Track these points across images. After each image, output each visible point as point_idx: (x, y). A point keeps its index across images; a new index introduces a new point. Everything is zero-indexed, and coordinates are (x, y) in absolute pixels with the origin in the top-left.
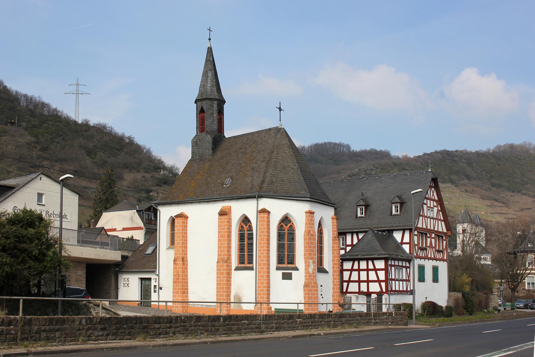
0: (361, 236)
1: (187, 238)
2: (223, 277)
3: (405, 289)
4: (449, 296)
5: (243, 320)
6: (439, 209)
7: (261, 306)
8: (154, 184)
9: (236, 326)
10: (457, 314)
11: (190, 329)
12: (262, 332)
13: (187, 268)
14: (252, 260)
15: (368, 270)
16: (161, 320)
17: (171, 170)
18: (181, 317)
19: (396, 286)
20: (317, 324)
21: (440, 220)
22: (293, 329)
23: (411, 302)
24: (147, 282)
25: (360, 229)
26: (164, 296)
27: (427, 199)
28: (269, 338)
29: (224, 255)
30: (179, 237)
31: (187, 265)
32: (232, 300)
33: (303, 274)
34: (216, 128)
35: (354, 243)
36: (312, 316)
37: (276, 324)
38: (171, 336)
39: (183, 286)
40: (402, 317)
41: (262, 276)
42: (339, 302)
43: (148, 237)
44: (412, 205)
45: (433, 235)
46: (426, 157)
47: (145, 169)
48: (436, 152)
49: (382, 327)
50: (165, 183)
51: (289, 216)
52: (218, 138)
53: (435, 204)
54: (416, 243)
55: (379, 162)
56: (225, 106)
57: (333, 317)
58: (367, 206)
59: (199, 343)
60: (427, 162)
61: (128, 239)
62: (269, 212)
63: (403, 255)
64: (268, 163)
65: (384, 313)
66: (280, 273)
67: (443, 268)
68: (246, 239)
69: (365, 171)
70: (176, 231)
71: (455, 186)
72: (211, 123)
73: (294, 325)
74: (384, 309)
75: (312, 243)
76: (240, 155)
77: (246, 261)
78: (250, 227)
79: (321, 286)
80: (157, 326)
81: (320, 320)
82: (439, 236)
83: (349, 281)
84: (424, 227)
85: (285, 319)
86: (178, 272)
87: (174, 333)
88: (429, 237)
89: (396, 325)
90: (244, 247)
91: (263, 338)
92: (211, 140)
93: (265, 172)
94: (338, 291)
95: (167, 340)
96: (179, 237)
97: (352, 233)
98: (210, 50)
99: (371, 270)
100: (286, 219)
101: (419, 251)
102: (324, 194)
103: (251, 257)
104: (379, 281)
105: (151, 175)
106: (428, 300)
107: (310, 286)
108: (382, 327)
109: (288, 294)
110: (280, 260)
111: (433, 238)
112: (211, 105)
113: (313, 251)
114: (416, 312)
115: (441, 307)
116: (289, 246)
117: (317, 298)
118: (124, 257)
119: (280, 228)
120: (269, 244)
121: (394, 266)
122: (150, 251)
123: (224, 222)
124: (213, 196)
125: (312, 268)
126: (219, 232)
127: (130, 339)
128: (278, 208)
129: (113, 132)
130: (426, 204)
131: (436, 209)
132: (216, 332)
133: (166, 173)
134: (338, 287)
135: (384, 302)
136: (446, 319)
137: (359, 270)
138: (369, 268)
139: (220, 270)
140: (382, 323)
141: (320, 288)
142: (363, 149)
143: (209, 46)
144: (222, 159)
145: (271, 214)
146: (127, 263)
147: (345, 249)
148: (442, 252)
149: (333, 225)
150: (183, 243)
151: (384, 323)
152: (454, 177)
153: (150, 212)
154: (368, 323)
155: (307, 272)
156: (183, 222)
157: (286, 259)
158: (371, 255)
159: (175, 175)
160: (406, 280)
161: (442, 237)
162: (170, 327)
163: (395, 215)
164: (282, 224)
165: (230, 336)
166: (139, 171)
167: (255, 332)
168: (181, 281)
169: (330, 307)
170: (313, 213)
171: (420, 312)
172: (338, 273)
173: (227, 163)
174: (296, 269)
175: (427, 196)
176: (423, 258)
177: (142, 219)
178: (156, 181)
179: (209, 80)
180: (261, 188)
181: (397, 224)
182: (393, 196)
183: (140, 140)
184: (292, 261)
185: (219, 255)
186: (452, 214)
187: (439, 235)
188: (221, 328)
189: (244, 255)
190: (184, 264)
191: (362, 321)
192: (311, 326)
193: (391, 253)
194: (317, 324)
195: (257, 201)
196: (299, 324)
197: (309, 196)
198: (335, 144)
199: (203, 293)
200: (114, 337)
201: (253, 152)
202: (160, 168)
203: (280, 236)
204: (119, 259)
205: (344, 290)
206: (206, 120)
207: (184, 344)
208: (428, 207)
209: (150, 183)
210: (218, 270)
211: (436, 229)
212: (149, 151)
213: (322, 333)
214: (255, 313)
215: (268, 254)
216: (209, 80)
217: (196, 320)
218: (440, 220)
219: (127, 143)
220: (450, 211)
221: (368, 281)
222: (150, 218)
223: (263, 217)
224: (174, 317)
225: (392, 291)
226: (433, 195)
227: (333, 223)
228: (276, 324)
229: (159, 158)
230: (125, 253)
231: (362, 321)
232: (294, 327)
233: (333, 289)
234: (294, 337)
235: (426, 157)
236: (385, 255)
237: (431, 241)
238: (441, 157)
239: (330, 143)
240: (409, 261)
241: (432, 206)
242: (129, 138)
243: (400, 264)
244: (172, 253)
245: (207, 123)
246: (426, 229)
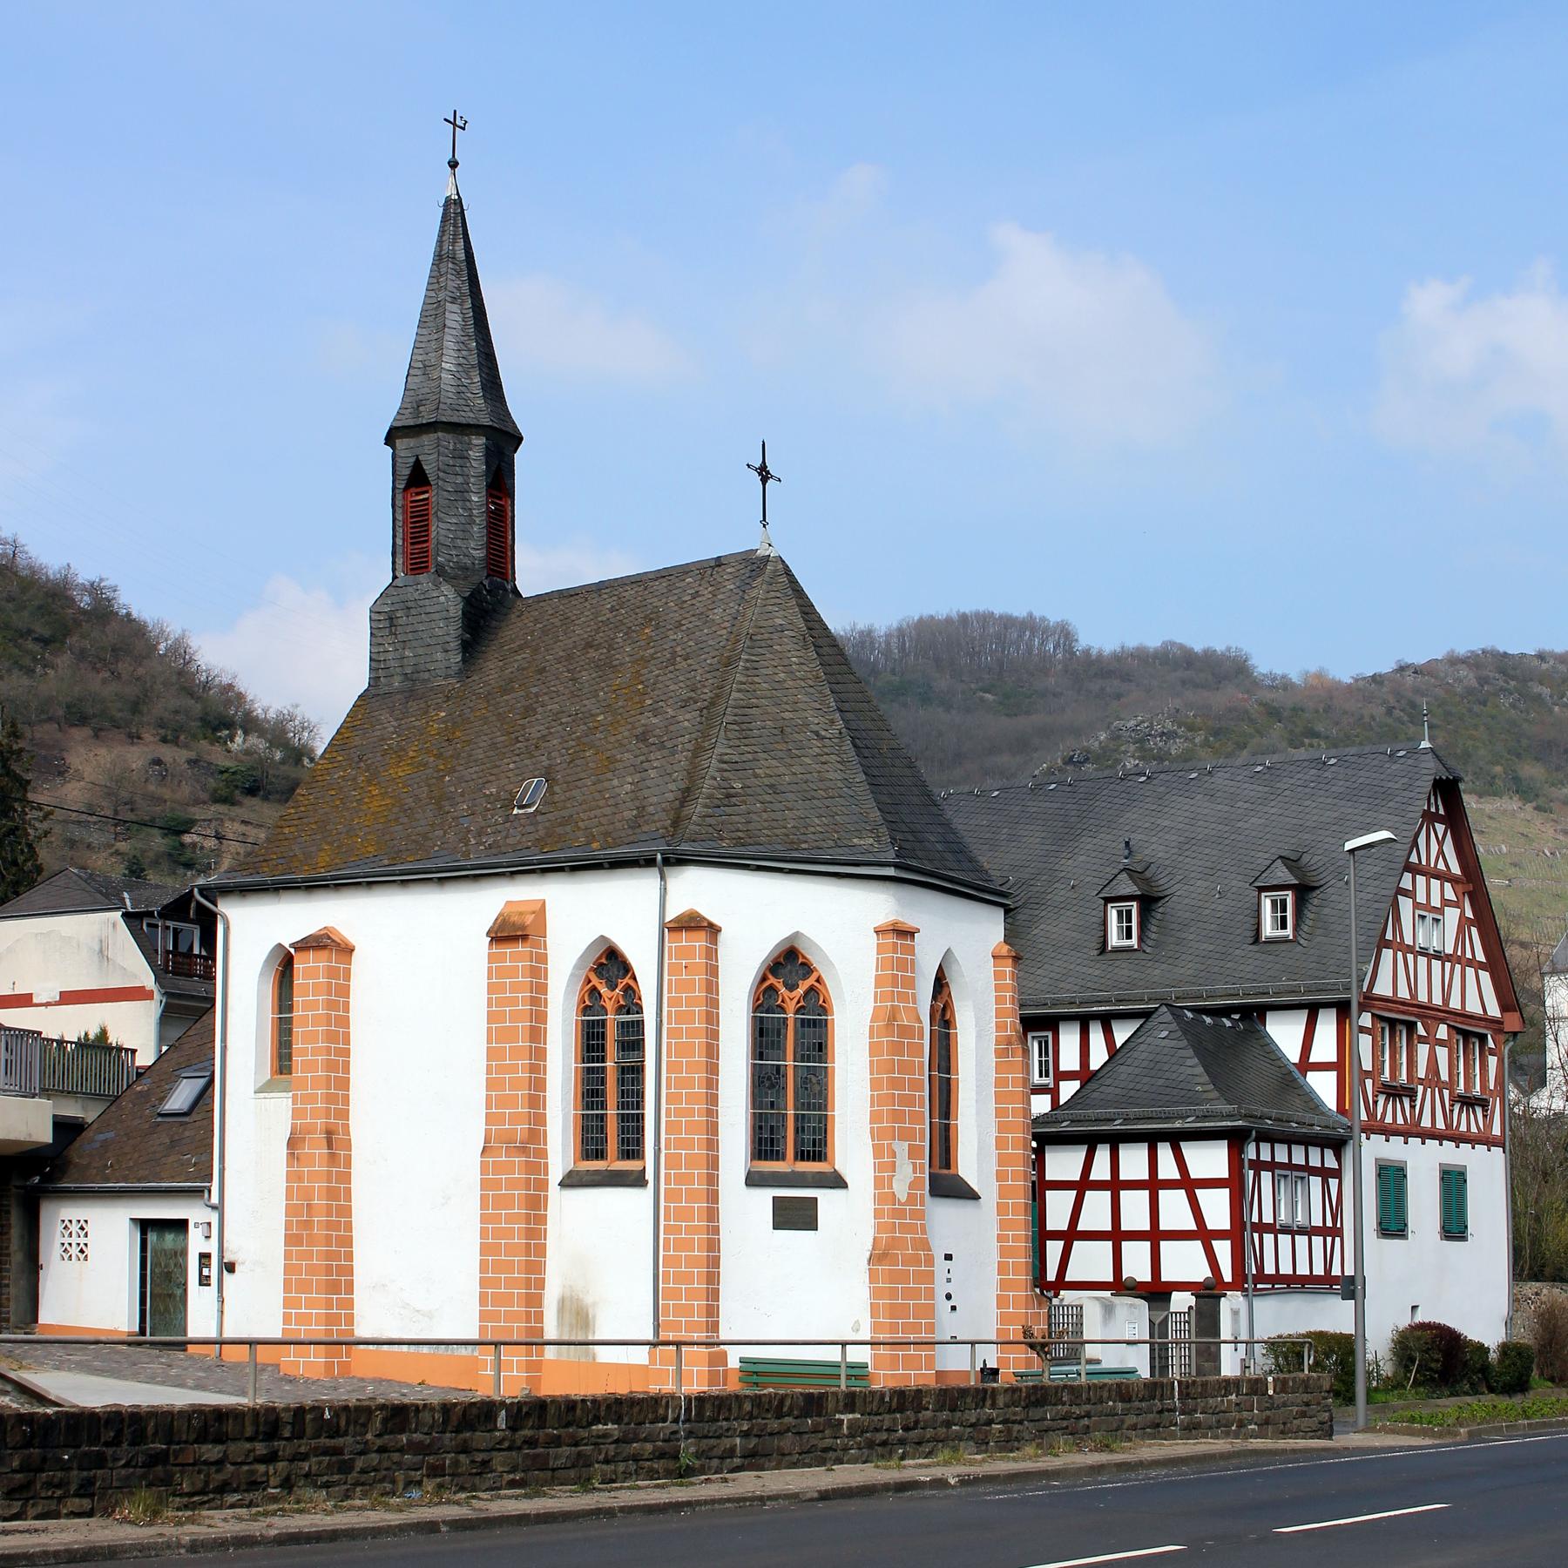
0: (1122, 1034)
1: (347, 1041)
2: (510, 1219)
3: (1319, 1270)
4: (1516, 1301)
5: (597, 1420)
6: (1469, 914)
7: (679, 1351)
8: (204, 796)
9: (566, 1450)
10: (1552, 1379)
11: (360, 1463)
12: (684, 1474)
13: (346, 1177)
14: (640, 1142)
15: (1153, 1185)
16: (230, 1427)
17: (278, 733)
18: (317, 1409)
19: (1279, 1255)
20: (929, 1433)
21: (1471, 963)
22: (822, 1457)
23: (1349, 1329)
24: (170, 1238)
25: (1120, 1001)
26: (245, 1302)
27: (1415, 870)
28: (713, 1501)
29: (514, 1119)
30: (310, 1037)
31: (348, 1164)
32: (551, 1333)
33: (869, 1206)
34: (480, 554)
35: (1095, 1064)
36: (905, 1400)
37: (746, 1435)
38: (274, 1499)
39: (330, 1256)
40: (1306, 1397)
41: (682, 1214)
42: (1027, 1332)
43: (175, 1033)
44: (1345, 900)
45: (1442, 1032)
46: (1409, 679)
47: (161, 724)
48: (1454, 661)
49: (1220, 1445)
50: (252, 791)
52: (489, 600)
53: (1450, 894)
54: (1367, 1065)
55: (1208, 709)
56: (523, 459)
57: (1001, 1401)
58: (1148, 903)
59: (402, 1529)
60: (1413, 705)
61: (83, 1045)
62: (713, 930)
63: (1308, 1117)
64: (709, 711)
65: (1227, 1381)
67: (1488, 1175)
69: (1141, 741)
70: (297, 1013)
71: (1537, 808)
72: (456, 531)
73: (828, 1442)
74: (1230, 1364)
75: (905, 1067)
76: (585, 676)
77: (612, 1145)
78: (631, 992)
79: (948, 1257)
80: (211, 1452)
81: (945, 1415)
82: (1467, 1035)
83: (1071, 1235)
84: (1404, 993)
85: (785, 1412)
86: (307, 1194)
87: (287, 1484)
88: (1422, 1040)
89: (1283, 1434)
90: (603, 1082)
91: (689, 1504)
92: (456, 609)
93: (698, 751)
94: (1024, 1277)
95: (254, 1518)
96: (310, 1037)
97: (1084, 1022)
98: (454, 214)
99: (1170, 1184)
100: (789, 962)
101: (1381, 1099)
102: (959, 850)
104: (1203, 1234)
105: (193, 755)
106: (1421, 1317)
107: (900, 1262)
108: (1220, 1445)
109: (802, 1296)
110: (764, 1144)
111: (1441, 1043)
112: (458, 455)
113: (909, 1101)
114: (1369, 1373)
115: (1481, 1349)
116: (805, 1081)
117: (930, 1311)
118: (66, 1129)
119: (764, 999)
120: (713, 1069)
121: (1272, 1166)
122: (181, 1097)
123: (512, 972)
124: (466, 855)
125: (908, 1174)
126: (492, 1017)
127: (90, 1514)
128: (755, 911)
129: (21, 561)
130: (1411, 894)
131: (1452, 916)
132: (476, 1476)
133: (256, 742)
134: (1023, 1260)
135: (1226, 1333)
136: (1503, 1402)
137: (1115, 1185)
138: (1161, 1176)
139: (496, 1185)
140: (1221, 1426)
141: (940, 1265)
142: (1132, 643)
143: (450, 192)
144: (505, 691)
145: (722, 937)
146: (80, 1152)
147: (1054, 1093)
148: (1483, 1103)
149: (998, 988)
150: (331, 1066)
151: (1228, 1425)
152: (1531, 771)
153: (186, 919)
154: (1157, 1429)
155: (884, 1194)
156: (332, 973)
157: (790, 1137)
158: (1168, 1119)
159: (298, 754)
160: (1322, 1231)
161: (1483, 1039)
162: (272, 1458)
163: (1272, 941)
164: (772, 980)
165: (538, 1494)
166: (134, 738)
167: (652, 1474)
168: (322, 1236)
169: (990, 1356)
171: (1387, 1369)
172: (1022, 1200)
173: (529, 711)
174: (836, 1182)
175: (1414, 859)
176: (1397, 1133)
177: (148, 951)
178: (212, 783)
179: (450, 344)
180: (676, 823)
181: (1285, 982)
182: (1262, 859)
183: (140, 600)
184: (815, 1146)
186: (1524, 934)
187: (1469, 1032)
188: (498, 1460)
189: (602, 1118)
190: (332, 1159)
191: (1131, 1419)
192: (902, 1442)
193: (1259, 1110)
194: (929, 1433)
195: (663, 878)
196: (851, 1436)
197: (890, 856)
198: (1007, 622)
199: (419, 1295)
200: (16, 1507)
201: (645, 661)
202: (230, 725)
203: (765, 1037)
204: (45, 1135)
205: (1051, 1276)
206: (433, 520)
207: (333, 1536)
208: (1416, 905)
209: (186, 791)
210: (485, 1184)
211: (1455, 1004)
212: (180, 651)
213: (951, 1473)
214: (654, 1389)
215: (712, 1112)
216: (450, 344)
217: (385, 1421)
218: (1471, 963)
219: (84, 612)
220: (1517, 919)
221: (1155, 1236)
222: (183, 948)
223: (689, 953)
224: (287, 1409)
225: (1261, 1277)
226: (1441, 852)
227: (998, 976)
228: (746, 1435)
229: (226, 680)
230: (72, 1110)
231: (1131, 1419)
232: (825, 1450)
233: (1002, 1268)
234: (825, 1496)
235: (1409, 679)
236: (1230, 1116)
237: (1434, 1055)
238: (1474, 683)
239: (985, 619)
240: (1337, 1145)
241: (1436, 902)
242: (94, 589)
243: (1298, 1159)
244: (279, 1111)
245: (439, 530)
246: (1412, 1005)
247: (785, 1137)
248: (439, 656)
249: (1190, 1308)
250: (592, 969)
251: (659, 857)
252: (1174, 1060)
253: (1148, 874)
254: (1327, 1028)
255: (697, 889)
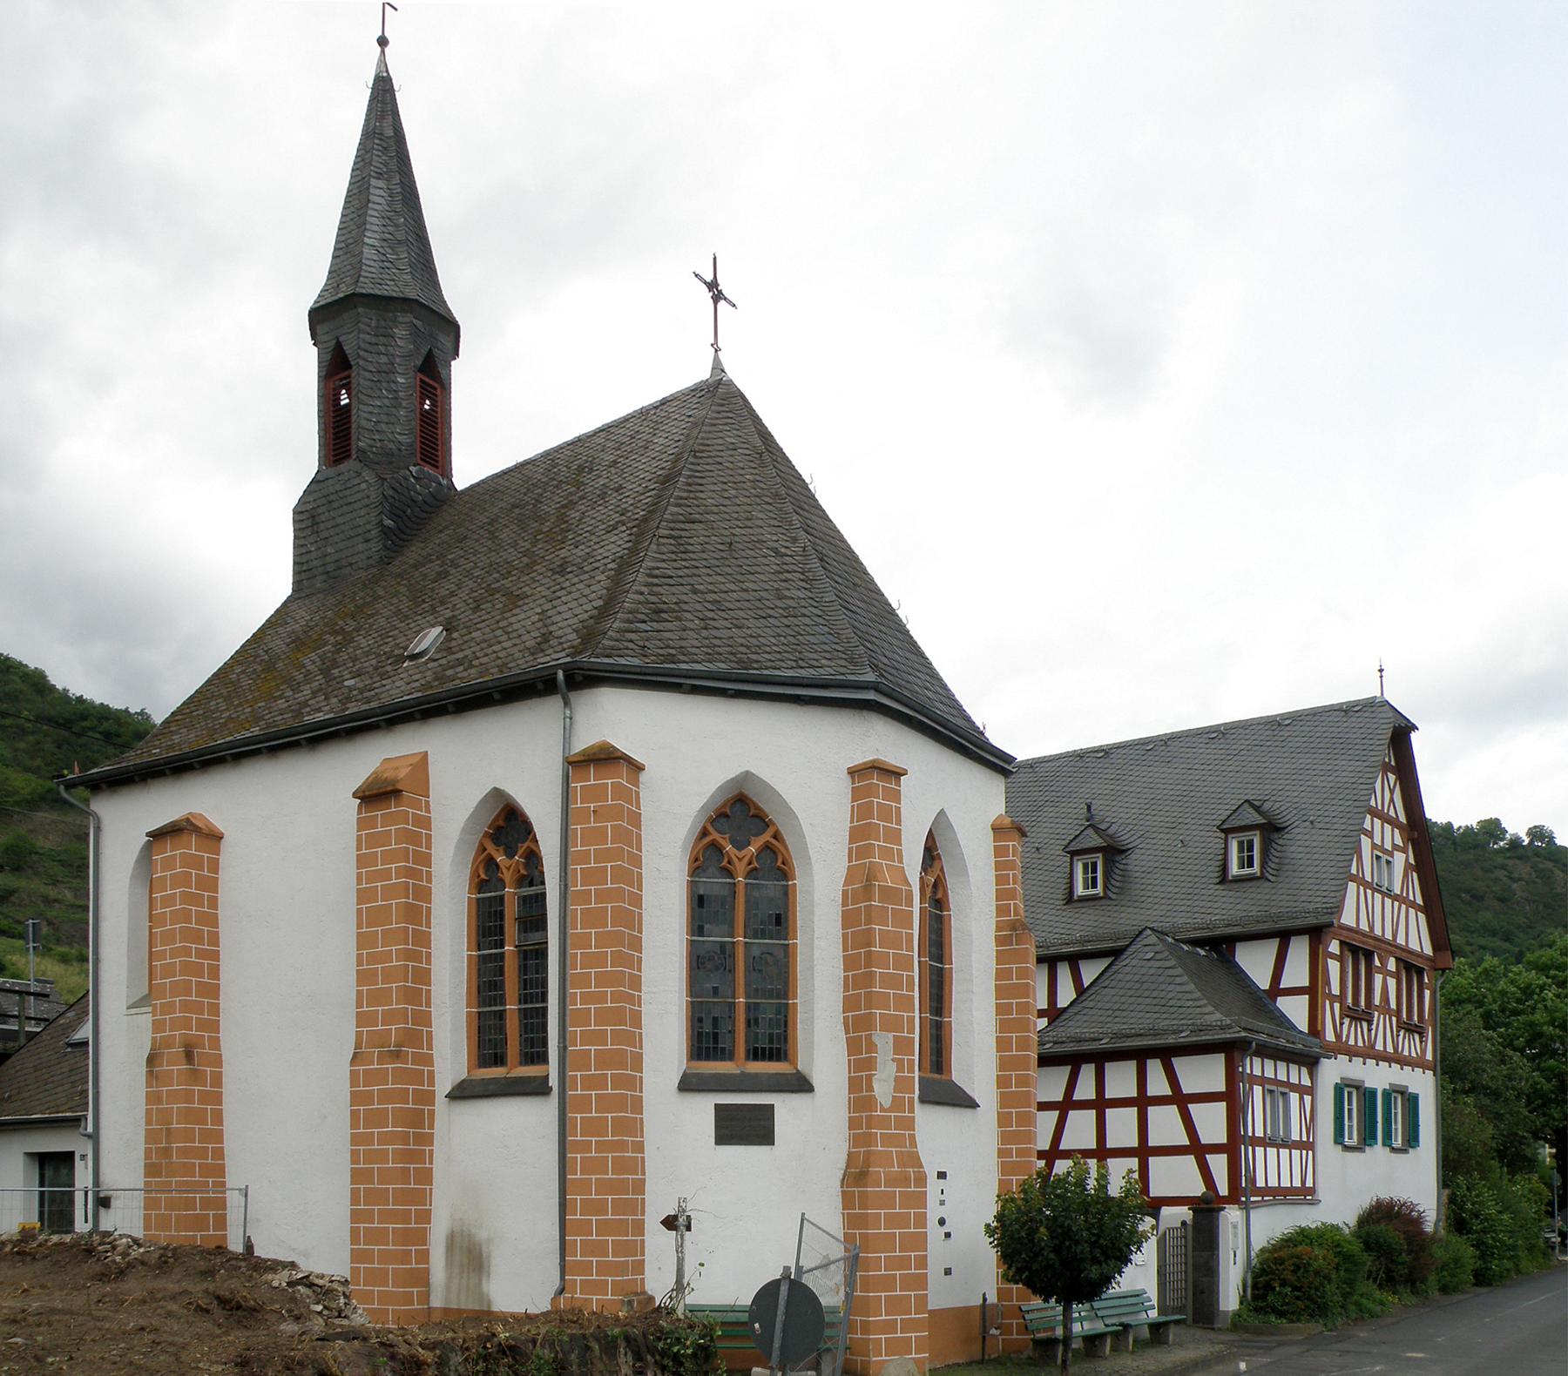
0: (1090, 972)
6: (1412, 861)
15: (1142, 1102)
21: (1413, 904)
29: (389, 1017)
45: (1392, 965)
51: (750, 794)
53: (1399, 841)
54: (1336, 990)
66: (703, 1109)
68: (511, 929)
72: (384, 422)
78: (533, 858)
79: (942, 1175)
83: (1102, 1152)
84: (1364, 926)
86: (165, 1117)
98: (383, 94)
99: (1161, 1101)
103: (534, 1022)
104: (1198, 1149)
107: (876, 1178)
110: (706, 1039)
112: (383, 330)
117: (920, 1241)
119: (707, 856)
121: (1263, 1081)
126: (363, 896)
130: (1370, 834)
131: (1399, 860)
137: (1101, 1104)
155: (860, 1084)
157: (743, 1035)
170: (896, 774)
174: (801, 1085)
184: (774, 1041)
185: (362, 1019)
195: (567, 703)
208: (1374, 846)
218: (1413, 904)
226: (1392, 800)
240: (1310, 1062)
241: (1388, 846)
246: (1370, 936)
247: (732, 1032)
248: (361, 547)
249: (1184, 1223)
250: (486, 834)
251: (560, 675)
252: (1161, 979)
253: (1111, 831)
254: (1299, 952)
255: (618, 717)
